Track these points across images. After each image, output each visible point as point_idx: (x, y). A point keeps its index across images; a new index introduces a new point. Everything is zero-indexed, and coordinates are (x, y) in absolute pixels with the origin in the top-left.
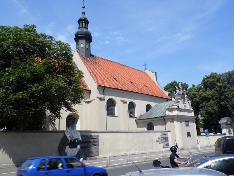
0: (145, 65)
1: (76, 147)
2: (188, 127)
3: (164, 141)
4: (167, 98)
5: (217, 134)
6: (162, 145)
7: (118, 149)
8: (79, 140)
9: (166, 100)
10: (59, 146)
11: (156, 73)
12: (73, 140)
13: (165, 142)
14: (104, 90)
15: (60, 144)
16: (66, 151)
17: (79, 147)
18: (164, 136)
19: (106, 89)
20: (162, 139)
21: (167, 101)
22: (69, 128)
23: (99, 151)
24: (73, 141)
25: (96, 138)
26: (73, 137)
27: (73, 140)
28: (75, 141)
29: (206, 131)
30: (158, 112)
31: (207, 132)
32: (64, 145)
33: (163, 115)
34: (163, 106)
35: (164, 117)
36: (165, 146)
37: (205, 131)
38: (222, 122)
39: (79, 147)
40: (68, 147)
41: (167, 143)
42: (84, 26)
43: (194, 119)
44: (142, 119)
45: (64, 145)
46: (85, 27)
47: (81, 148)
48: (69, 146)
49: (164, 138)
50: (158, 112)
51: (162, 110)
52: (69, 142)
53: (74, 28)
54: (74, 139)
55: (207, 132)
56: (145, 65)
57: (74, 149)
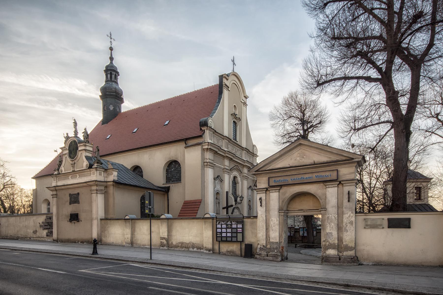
6: (45, 232)
18: (49, 221)
20: (47, 224)
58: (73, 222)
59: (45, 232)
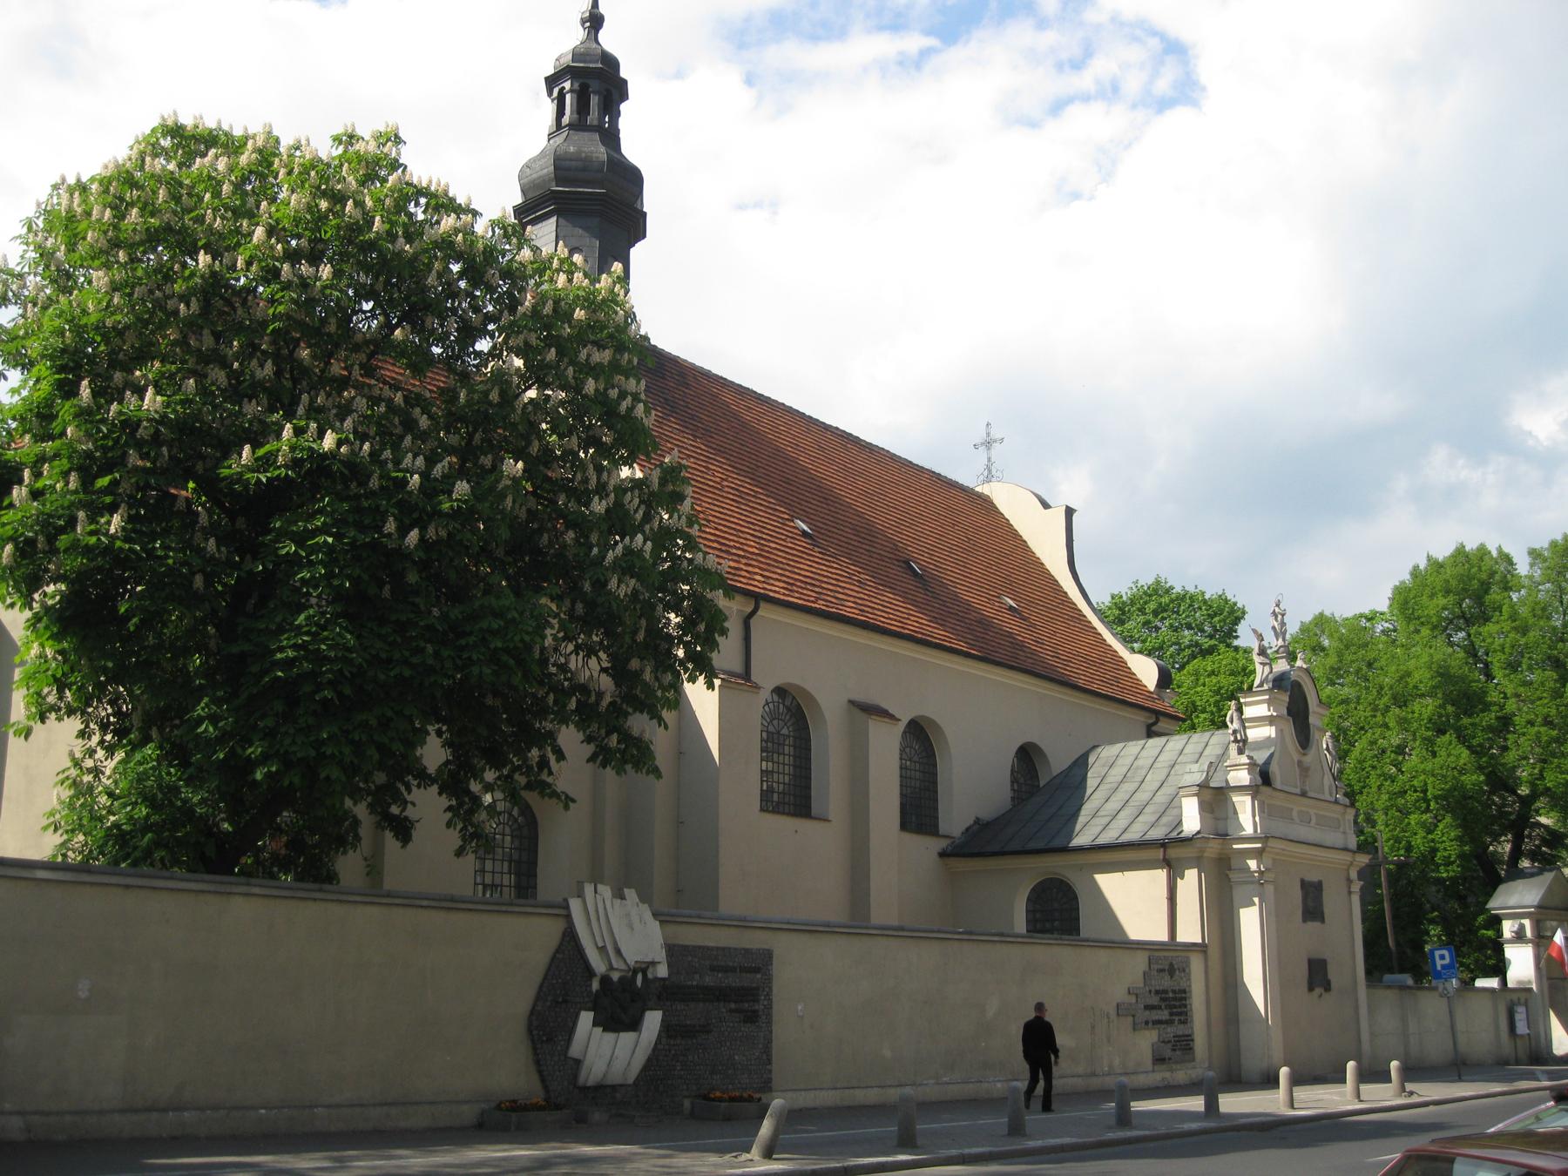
0: (988, 444)
1: (634, 1025)
2: (1313, 926)
3: (1164, 1015)
4: (1149, 704)
5: (1388, 977)
6: (1146, 1040)
7: (887, 1053)
8: (657, 979)
9: (1142, 718)
10: (532, 1012)
11: (1070, 512)
12: (615, 976)
13: (1169, 1022)
14: (752, 621)
15: (539, 997)
16: (575, 1051)
17: (653, 1020)
18: (1166, 983)
19: (765, 611)
20: (1155, 1000)
21: (1150, 733)
22: (600, 887)
23: (769, 1062)
24: (621, 979)
25: (757, 970)
26: (618, 952)
27: (615, 976)
28: (627, 982)
29: (1442, 957)
30: (1113, 805)
31: (1447, 961)
32: (565, 1001)
33: (1157, 833)
34: (1144, 762)
35: (1163, 844)
36: (1168, 1053)
37: (1437, 953)
38: (1512, 901)
39: (653, 1020)
40: (586, 1018)
41: (1181, 1030)
42: (593, 117)
43: (1354, 875)
44: (1041, 845)
45: (565, 1001)
46: (598, 128)
47: (667, 1029)
48: (591, 1015)
49: (1165, 992)
50: (1113, 805)
51: (1142, 796)
52: (595, 985)
53: (528, 131)
54: (623, 967)
55: (1447, 961)
56: (988, 444)
57: (627, 1038)
58: (1318, 991)
59: (1146, 1040)
